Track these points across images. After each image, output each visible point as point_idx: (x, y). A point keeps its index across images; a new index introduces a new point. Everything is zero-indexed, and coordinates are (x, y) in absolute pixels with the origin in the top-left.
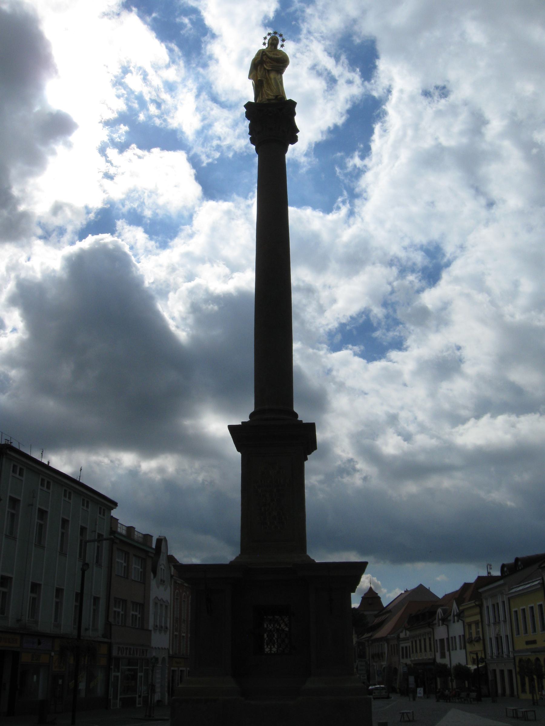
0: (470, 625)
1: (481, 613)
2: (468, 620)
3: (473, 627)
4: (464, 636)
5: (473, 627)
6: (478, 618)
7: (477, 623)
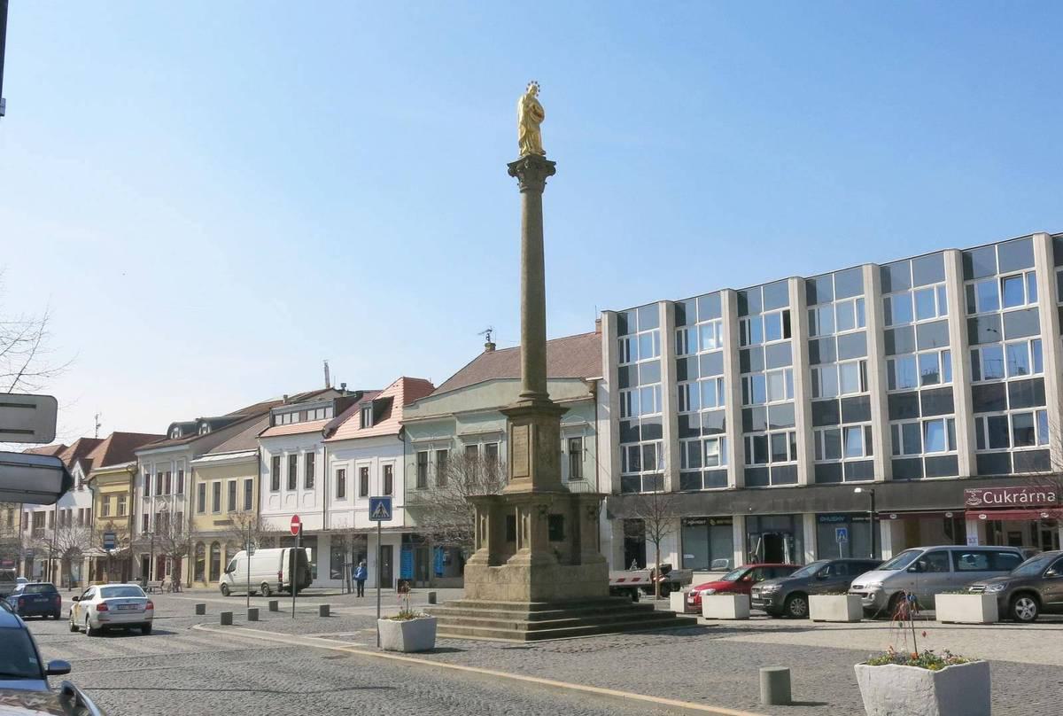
0: (106, 497)
2: (104, 490)
5: (113, 501)
6: (126, 488)
7: (121, 496)
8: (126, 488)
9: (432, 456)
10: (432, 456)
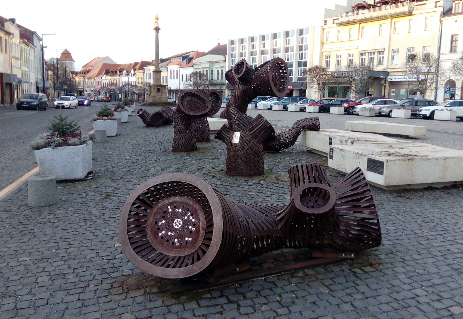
1: (144, 75)
2: (138, 77)
3: (140, 79)
4: (136, 82)
5: (140, 79)
7: (142, 78)
8: (143, 76)
9: (220, 72)
10: (220, 72)
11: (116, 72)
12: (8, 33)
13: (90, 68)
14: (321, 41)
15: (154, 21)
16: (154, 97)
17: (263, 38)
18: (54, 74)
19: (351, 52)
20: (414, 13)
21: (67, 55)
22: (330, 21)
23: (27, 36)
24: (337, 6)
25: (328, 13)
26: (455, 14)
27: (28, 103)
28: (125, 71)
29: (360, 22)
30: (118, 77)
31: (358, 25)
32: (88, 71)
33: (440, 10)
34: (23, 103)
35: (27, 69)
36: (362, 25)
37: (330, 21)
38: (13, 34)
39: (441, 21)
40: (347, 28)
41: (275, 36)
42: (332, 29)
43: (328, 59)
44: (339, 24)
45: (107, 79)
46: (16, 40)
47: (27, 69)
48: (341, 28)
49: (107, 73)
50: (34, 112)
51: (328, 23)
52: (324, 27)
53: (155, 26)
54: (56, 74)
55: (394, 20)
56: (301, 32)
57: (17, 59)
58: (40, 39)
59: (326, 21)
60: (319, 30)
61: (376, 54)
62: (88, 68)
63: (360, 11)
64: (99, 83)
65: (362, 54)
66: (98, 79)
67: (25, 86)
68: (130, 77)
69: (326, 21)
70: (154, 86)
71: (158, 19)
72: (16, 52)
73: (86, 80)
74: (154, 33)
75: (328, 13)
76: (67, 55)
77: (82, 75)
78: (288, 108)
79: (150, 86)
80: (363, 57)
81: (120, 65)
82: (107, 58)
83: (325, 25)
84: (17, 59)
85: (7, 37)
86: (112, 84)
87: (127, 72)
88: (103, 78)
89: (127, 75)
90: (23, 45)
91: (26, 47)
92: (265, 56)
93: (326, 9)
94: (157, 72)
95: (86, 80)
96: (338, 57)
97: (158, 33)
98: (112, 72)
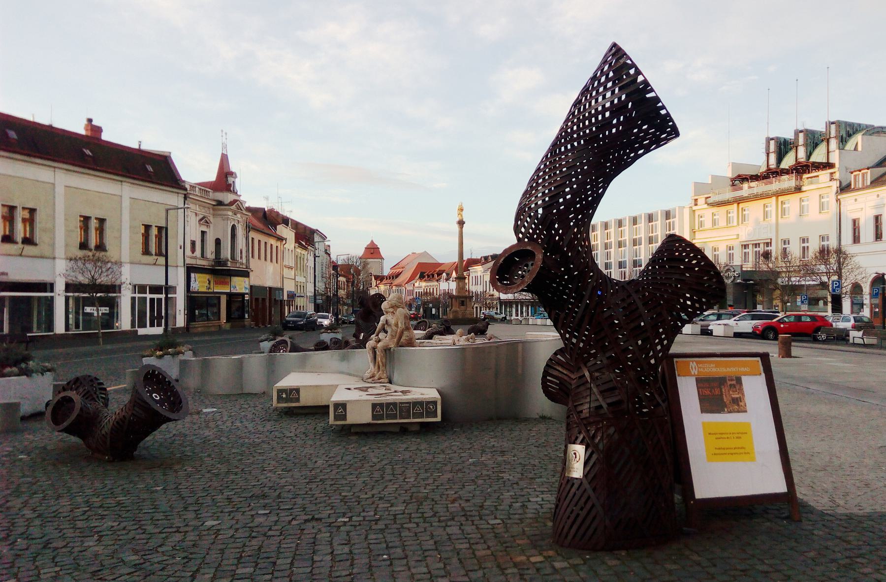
11: (433, 276)
12: (280, 239)
13: (401, 270)
14: (690, 227)
15: (456, 212)
16: (456, 312)
17: (620, 223)
18: (347, 281)
19: (730, 244)
20: (804, 188)
21: (373, 251)
22: (701, 201)
23: (306, 236)
24: (714, 177)
25: (699, 188)
26: (855, 190)
27: (294, 322)
28: (444, 274)
29: (778, 194)
30: (436, 283)
31: (736, 205)
32: (398, 275)
33: (835, 185)
34: (289, 322)
35: (303, 280)
36: (741, 205)
37: (701, 201)
38: (286, 239)
39: (838, 200)
40: (723, 209)
41: (635, 221)
42: (707, 213)
43: (731, 252)
44: (712, 205)
45: (421, 286)
46: (291, 244)
47: (303, 280)
48: (715, 210)
49: (422, 277)
50: (299, 332)
51: (699, 202)
52: (695, 208)
53: (457, 219)
54: (351, 282)
55: (781, 198)
56: (668, 215)
57: (291, 268)
58: (324, 238)
59: (696, 200)
60: (687, 212)
61: (750, 246)
62: (398, 271)
63: (745, 185)
64: (411, 292)
65: (745, 246)
66: (409, 287)
67: (299, 302)
68: (450, 282)
69: (696, 200)
70: (456, 297)
71: (462, 210)
72: (289, 260)
73: (394, 288)
74: (456, 228)
75: (699, 188)
76: (373, 251)
77: (389, 281)
78: (711, 331)
79: (451, 296)
80: (747, 250)
81: (440, 265)
82: (425, 254)
83: (696, 205)
84: (291, 268)
85: (279, 244)
86: (426, 294)
87: (448, 274)
88: (417, 285)
89: (447, 280)
90: (299, 250)
91: (304, 252)
92: (623, 249)
93: (695, 183)
94: (461, 279)
95: (394, 288)
96: (804, 242)
97: (462, 228)
98: (428, 276)
